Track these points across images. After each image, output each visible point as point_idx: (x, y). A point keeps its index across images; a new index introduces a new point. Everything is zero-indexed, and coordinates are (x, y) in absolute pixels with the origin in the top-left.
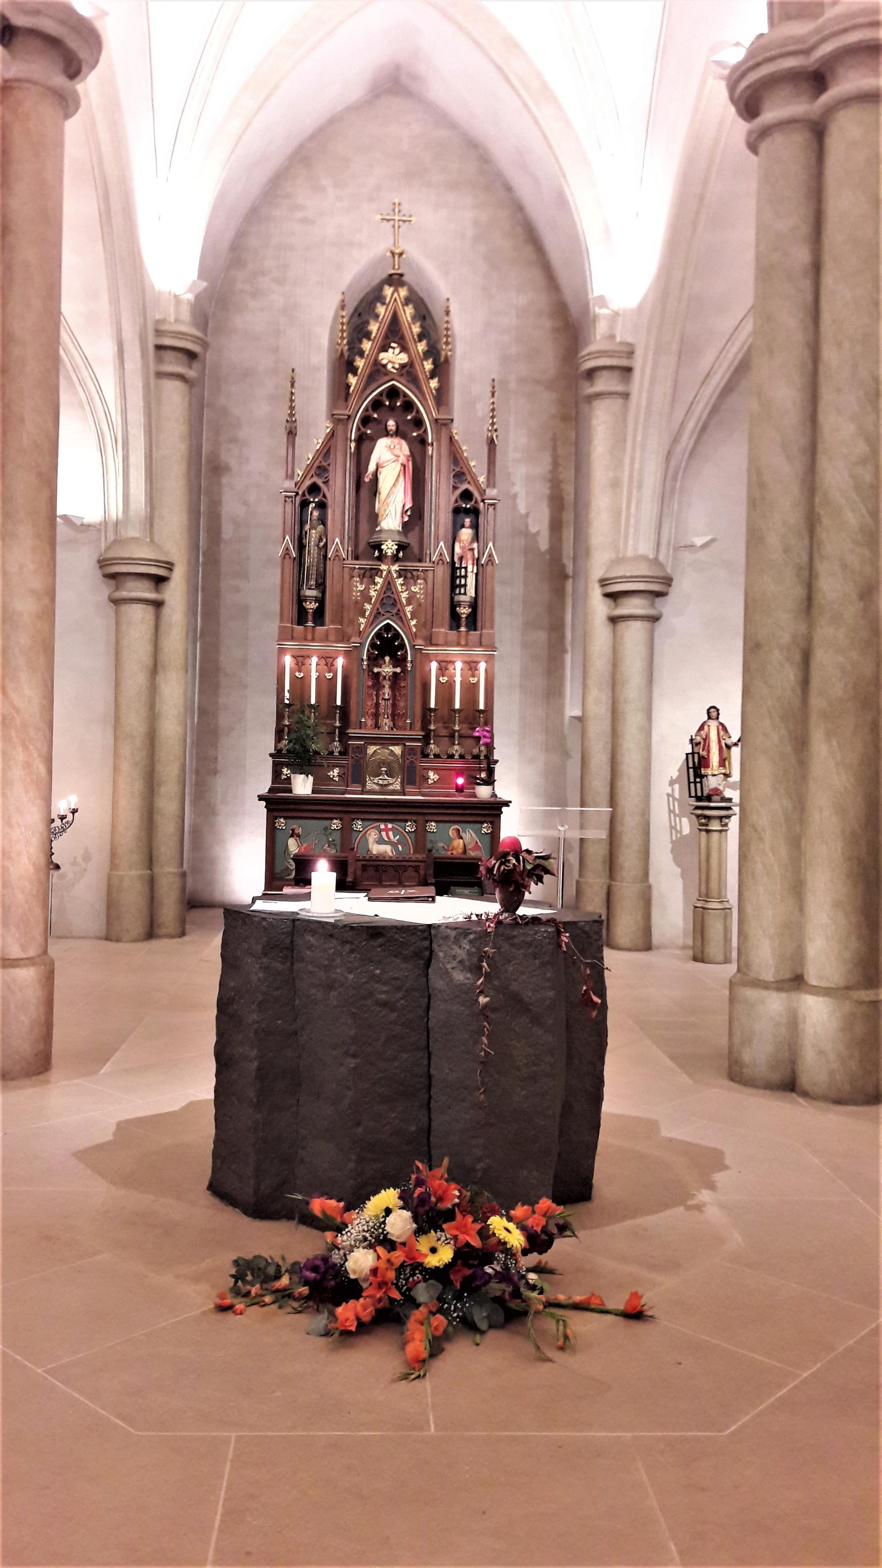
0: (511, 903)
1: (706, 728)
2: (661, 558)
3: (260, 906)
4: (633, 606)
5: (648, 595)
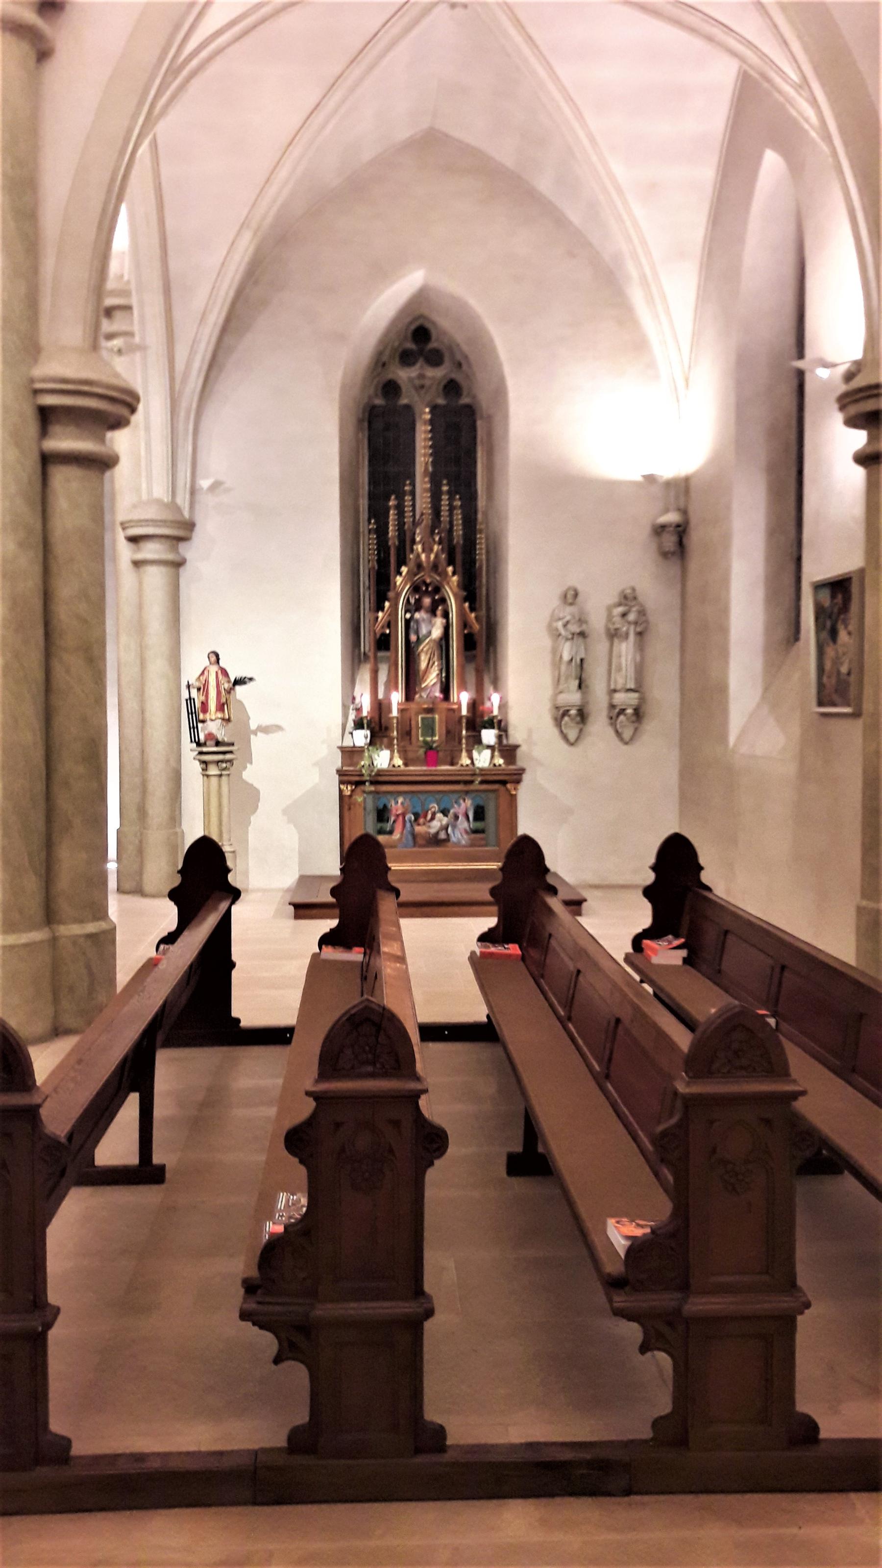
0: (642, 981)
1: (206, 673)
2: (179, 501)
3: (223, 906)
4: (151, 551)
5: (163, 540)
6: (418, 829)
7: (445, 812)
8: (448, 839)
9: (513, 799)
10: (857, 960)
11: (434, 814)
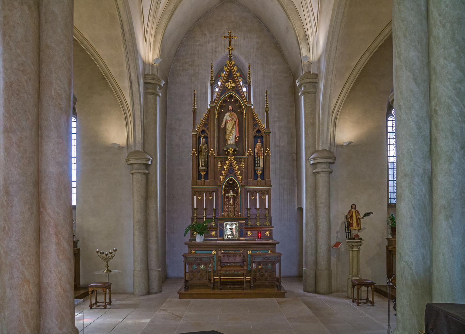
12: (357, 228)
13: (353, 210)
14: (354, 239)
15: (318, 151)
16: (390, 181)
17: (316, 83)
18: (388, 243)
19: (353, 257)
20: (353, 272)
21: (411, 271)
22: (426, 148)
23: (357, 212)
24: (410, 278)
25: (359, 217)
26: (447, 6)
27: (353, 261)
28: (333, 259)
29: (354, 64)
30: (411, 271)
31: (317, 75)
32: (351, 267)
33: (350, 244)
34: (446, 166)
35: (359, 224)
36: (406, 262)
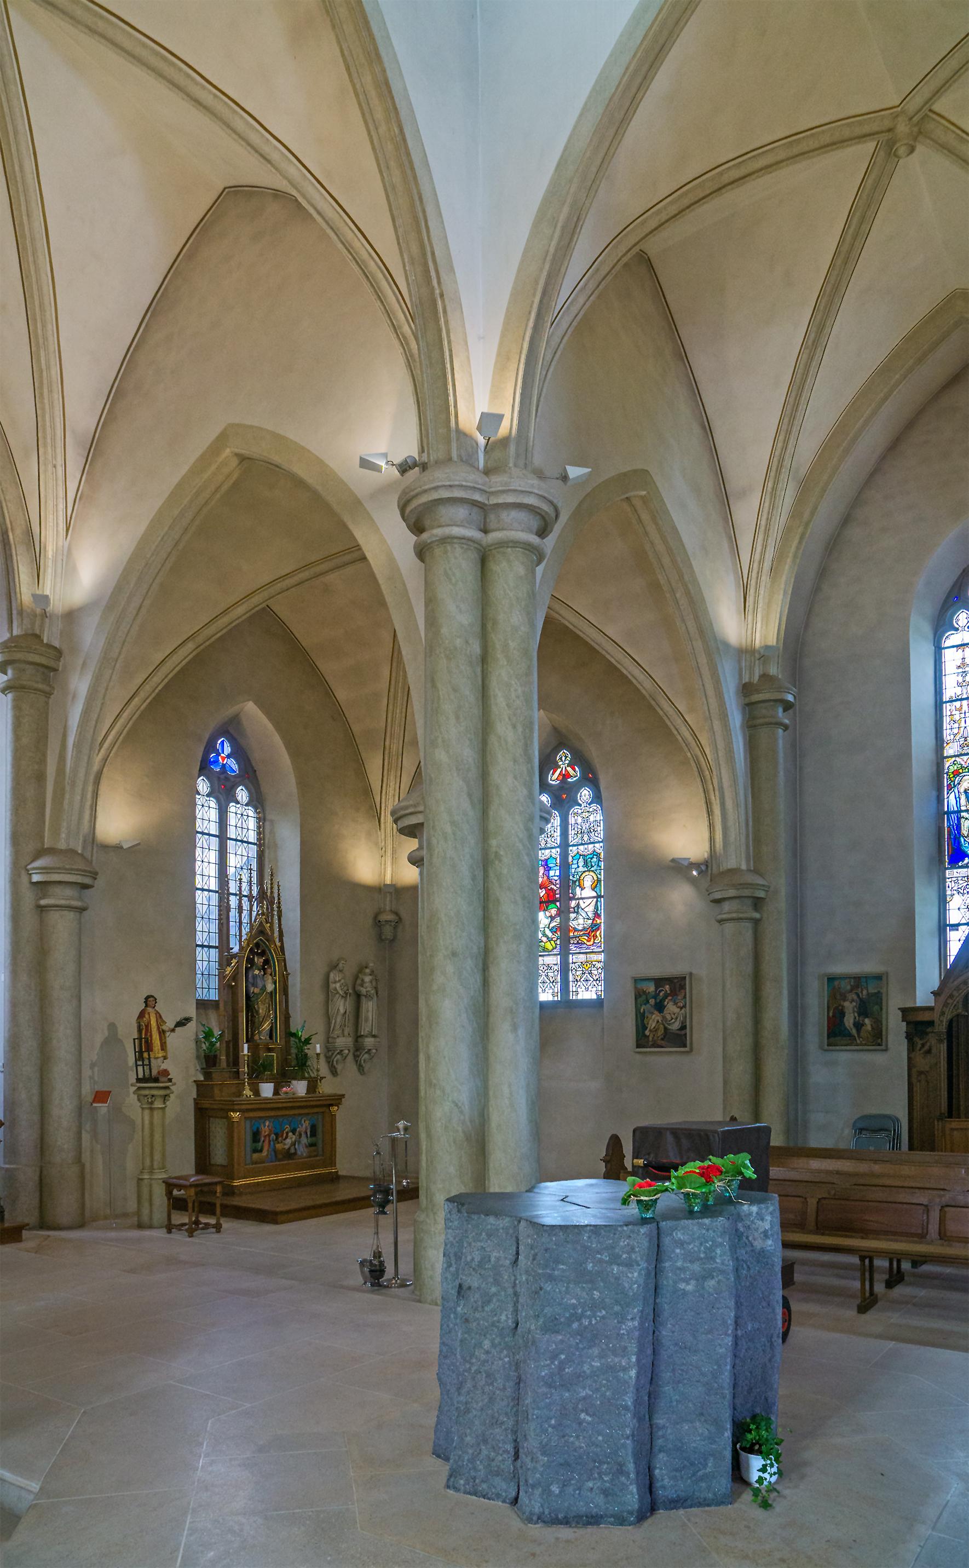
6: (279, 1146)
7: (294, 1131)
8: (295, 1154)
9: (333, 1117)
10: (748, 1458)
11: (287, 1133)
12: (161, 1054)
13: (150, 1009)
14: (156, 1080)
15: (51, 851)
16: (215, 947)
17: (55, 670)
18: (198, 1091)
19: (151, 1123)
20: (152, 1161)
21: (462, 1118)
22: (480, 912)
23: (159, 1016)
24: (460, 1129)
25: (164, 1027)
26: (518, 697)
27: (152, 1135)
28: (86, 1137)
29: (160, 657)
30: (462, 1118)
31: (59, 653)
32: (147, 1150)
33: (146, 1092)
34: (515, 946)
35: (163, 1046)
36: (454, 1102)
